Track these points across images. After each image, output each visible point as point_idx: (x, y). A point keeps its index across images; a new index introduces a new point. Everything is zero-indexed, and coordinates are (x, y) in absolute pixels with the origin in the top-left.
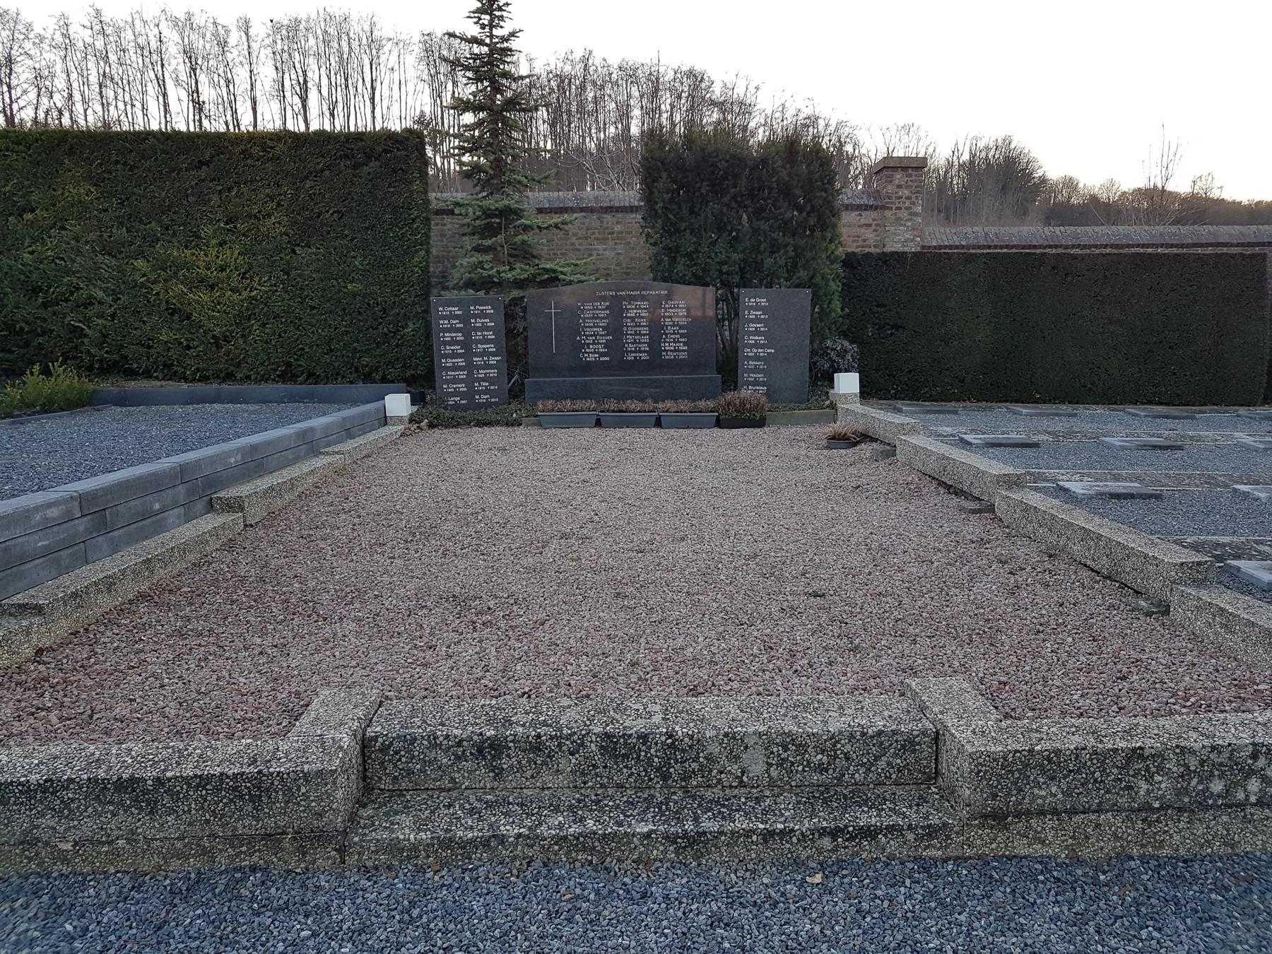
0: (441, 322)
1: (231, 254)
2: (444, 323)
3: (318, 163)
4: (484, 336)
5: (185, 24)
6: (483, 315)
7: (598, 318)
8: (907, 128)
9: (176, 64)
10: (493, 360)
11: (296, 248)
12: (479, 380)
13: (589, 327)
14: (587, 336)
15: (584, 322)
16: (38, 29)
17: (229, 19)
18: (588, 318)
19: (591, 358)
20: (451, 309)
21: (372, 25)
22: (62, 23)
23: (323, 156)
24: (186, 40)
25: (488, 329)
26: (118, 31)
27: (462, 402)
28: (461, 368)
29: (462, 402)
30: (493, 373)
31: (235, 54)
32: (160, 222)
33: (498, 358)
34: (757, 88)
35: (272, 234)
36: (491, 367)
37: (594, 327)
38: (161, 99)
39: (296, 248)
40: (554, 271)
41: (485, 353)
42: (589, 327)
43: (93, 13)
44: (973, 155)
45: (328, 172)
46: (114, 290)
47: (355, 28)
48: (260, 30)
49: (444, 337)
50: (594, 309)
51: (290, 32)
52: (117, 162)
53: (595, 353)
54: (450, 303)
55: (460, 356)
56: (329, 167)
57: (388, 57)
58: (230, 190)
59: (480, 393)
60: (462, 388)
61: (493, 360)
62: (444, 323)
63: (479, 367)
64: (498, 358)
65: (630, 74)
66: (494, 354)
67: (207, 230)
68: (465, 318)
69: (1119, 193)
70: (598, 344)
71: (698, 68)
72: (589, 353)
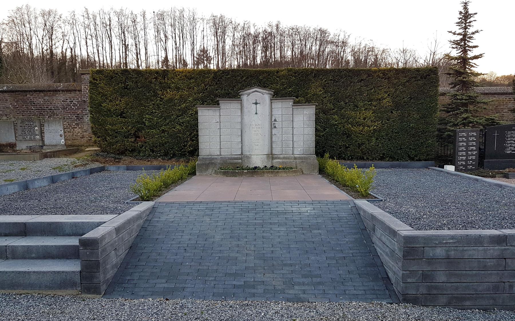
0: (460, 139)
1: (369, 114)
2: (461, 139)
3: (404, 80)
4: (472, 144)
5: (120, 14)
6: (473, 136)
7: (512, 137)
8: (404, 51)
9: (116, 31)
10: (475, 153)
11: (393, 111)
12: (470, 160)
13: (509, 140)
14: (508, 144)
15: (507, 139)
16: (63, 17)
17: (137, 11)
18: (509, 137)
19: (509, 152)
20: (463, 134)
21: (193, 13)
22: (72, 14)
23: (406, 77)
24: (120, 20)
25: (474, 141)
26: (95, 17)
27: (473, 168)
28: (464, 156)
29: (473, 168)
30: (474, 157)
31: (140, 26)
32: (344, 101)
33: (476, 152)
34: (349, 36)
35: (385, 106)
36: (473, 155)
37: (511, 140)
38: (110, 43)
39: (393, 111)
40: (493, 119)
41: (472, 150)
42: (509, 140)
43: (84, 10)
44: (433, 62)
45: (408, 83)
46: (324, 126)
47: (186, 14)
48: (149, 16)
49: (460, 144)
50: (511, 134)
51: (161, 16)
52: (331, 80)
53: (510, 150)
54: (463, 132)
55: (464, 151)
56: (407, 81)
57: (199, 26)
58: (371, 89)
59: (469, 165)
60: (464, 163)
61: (475, 153)
62: (461, 139)
63: (470, 155)
64: (476, 152)
65: (296, 31)
66: (475, 151)
67: (361, 104)
68: (467, 137)
69: (495, 77)
70: (512, 147)
71: (324, 28)
72: (508, 150)
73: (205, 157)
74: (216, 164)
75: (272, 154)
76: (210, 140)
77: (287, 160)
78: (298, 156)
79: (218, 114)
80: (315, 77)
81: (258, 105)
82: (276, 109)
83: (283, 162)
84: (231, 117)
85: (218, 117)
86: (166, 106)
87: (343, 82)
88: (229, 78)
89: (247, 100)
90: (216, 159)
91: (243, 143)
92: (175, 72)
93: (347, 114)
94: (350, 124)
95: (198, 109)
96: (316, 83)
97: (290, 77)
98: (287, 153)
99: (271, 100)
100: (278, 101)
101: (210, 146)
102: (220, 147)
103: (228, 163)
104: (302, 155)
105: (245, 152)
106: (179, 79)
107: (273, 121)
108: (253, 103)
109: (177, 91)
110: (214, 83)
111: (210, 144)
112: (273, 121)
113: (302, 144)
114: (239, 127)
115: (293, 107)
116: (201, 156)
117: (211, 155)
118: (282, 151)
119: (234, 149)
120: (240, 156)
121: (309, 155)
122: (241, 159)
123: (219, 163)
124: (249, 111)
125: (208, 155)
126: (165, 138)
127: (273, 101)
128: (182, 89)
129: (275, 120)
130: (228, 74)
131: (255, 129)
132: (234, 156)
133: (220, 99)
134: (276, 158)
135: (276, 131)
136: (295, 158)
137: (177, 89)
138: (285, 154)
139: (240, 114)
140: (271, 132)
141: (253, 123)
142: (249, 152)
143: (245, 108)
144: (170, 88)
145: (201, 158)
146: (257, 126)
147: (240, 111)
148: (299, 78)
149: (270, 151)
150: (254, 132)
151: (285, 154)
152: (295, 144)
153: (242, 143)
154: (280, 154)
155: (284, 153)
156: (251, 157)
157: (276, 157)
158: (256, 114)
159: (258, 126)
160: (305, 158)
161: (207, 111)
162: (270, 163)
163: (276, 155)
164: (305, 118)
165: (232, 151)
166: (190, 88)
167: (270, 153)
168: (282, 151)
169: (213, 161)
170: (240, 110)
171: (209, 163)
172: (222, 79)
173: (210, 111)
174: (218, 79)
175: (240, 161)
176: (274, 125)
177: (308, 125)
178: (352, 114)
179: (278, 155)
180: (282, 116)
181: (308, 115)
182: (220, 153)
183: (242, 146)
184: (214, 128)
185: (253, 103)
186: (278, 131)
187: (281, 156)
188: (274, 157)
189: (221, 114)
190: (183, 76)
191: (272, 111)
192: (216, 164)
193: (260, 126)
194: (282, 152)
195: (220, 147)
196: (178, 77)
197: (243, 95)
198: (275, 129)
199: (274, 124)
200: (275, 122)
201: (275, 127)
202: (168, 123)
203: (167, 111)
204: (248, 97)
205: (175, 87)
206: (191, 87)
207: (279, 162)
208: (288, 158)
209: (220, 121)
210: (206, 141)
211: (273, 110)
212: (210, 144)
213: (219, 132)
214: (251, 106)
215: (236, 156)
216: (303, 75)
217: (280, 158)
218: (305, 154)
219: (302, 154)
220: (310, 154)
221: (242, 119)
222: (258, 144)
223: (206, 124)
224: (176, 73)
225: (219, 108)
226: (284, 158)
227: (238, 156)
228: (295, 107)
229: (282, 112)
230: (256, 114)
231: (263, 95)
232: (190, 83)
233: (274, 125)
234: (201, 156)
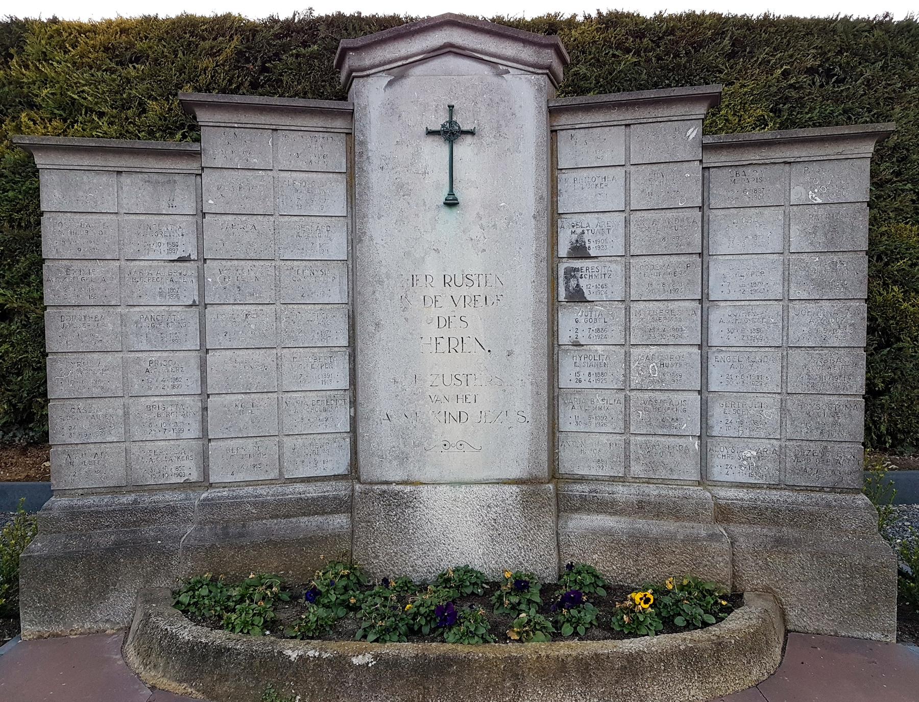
52: (811, 71)
73: (91, 500)
74: (163, 554)
75: (554, 475)
76: (126, 383)
77: (669, 526)
78: (742, 494)
79: (190, 208)
80: (732, 55)
81: (464, 149)
82: (585, 173)
83: (637, 540)
84: (57, 141)
85: (187, 224)
86: (11, 194)
87: (868, 83)
88: (313, 56)
89: (392, 110)
90: (172, 510)
91: (360, 399)
92: (57, 31)
93: (882, 234)
94: (895, 282)
95: (40, 160)
96: (743, 86)
97: (614, 56)
98: (663, 474)
99: (553, 112)
100: (599, 117)
101: (126, 424)
102: (205, 430)
103: (255, 546)
104: (775, 495)
105: (376, 460)
106: (74, 63)
107: (563, 251)
108: (430, 133)
109: (65, 120)
110: (242, 84)
111: (126, 414)
112: (563, 251)
113: (771, 414)
114: (337, 293)
115: (712, 159)
116: (63, 493)
117: (140, 488)
118: (627, 457)
119: (300, 441)
120: (341, 489)
121: (821, 489)
122: (346, 505)
123: (186, 548)
124: (401, 186)
125: (116, 490)
126: (12, 345)
127: (564, 120)
128: (89, 110)
129: (579, 251)
130: (314, 38)
131: (446, 309)
132: (300, 487)
133: (202, 97)
134: (587, 505)
135: (583, 325)
136: (724, 513)
137: (64, 110)
138: (649, 481)
139: (339, 206)
140: (553, 333)
141: (432, 267)
142: (403, 459)
143: (376, 162)
144: (31, 105)
145: (55, 513)
146: (454, 291)
147: (339, 188)
148: (659, 58)
149: (544, 457)
150: (433, 331)
151: (649, 481)
152: (717, 412)
153: (354, 403)
154: (613, 480)
155: (637, 469)
156: (413, 497)
157: (583, 499)
158: (451, 203)
159: (464, 291)
160: (795, 516)
161: (104, 178)
162: (545, 536)
163: (582, 479)
164: (795, 231)
165: (287, 454)
166: (125, 107)
167: (543, 471)
168: (627, 457)
169: (148, 531)
170: (342, 179)
171: (118, 545)
172: (280, 60)
173: (126, 180)
174: (264, 63)
175: (340, 521)
176: (573, 283)
177: (820, 285)
178: (909, 237)
179: (596, 480)
180: (627, 222)
181: (821, 211)
182: (205, 471)
183: (354, 421)
184: (158, 301)
185: (430, 133)
186: (600, 324)
187: (622, 492)
188: (570, 498)
189: (210, 204)
190: (94, 47)
191: (554, 191)
192: (170, 554)
193: (475, 290)
194: (627, 467)
195: (205, 430)
196: (73, 52)
197: (364, 72)
198: (579, 311)
199: (571, 273)
200: (577, 264)
201: (577, 297)
202: (26, 275)
203: (16, 216)
204: (397, 87)
205: (55, 101)
206: (130, 99)
207: (609, 533)
208: (674, 511)
209: (200, 249)
210: (96, 392)
211: (566, 182)
212: (126, 414)
213: (194, 326)
214: (417, 154)
215: (312, 491)
216: (677, 42)
217: (614, 503)
218: (792, 488)
219: (770, 487)
220: (833, 490)
221: (355, 239)
222: (462, 406)
223: (98, 270)
224: (60, 34)
225: (193, 166)
226: (641, 507)
227: (329, 489)
228: (723, 158)
229: (627, 190)
230: (451, 203)
231: (500, 74)
232: (128, 81)
233: (573, 283)
234: (63, 493)
